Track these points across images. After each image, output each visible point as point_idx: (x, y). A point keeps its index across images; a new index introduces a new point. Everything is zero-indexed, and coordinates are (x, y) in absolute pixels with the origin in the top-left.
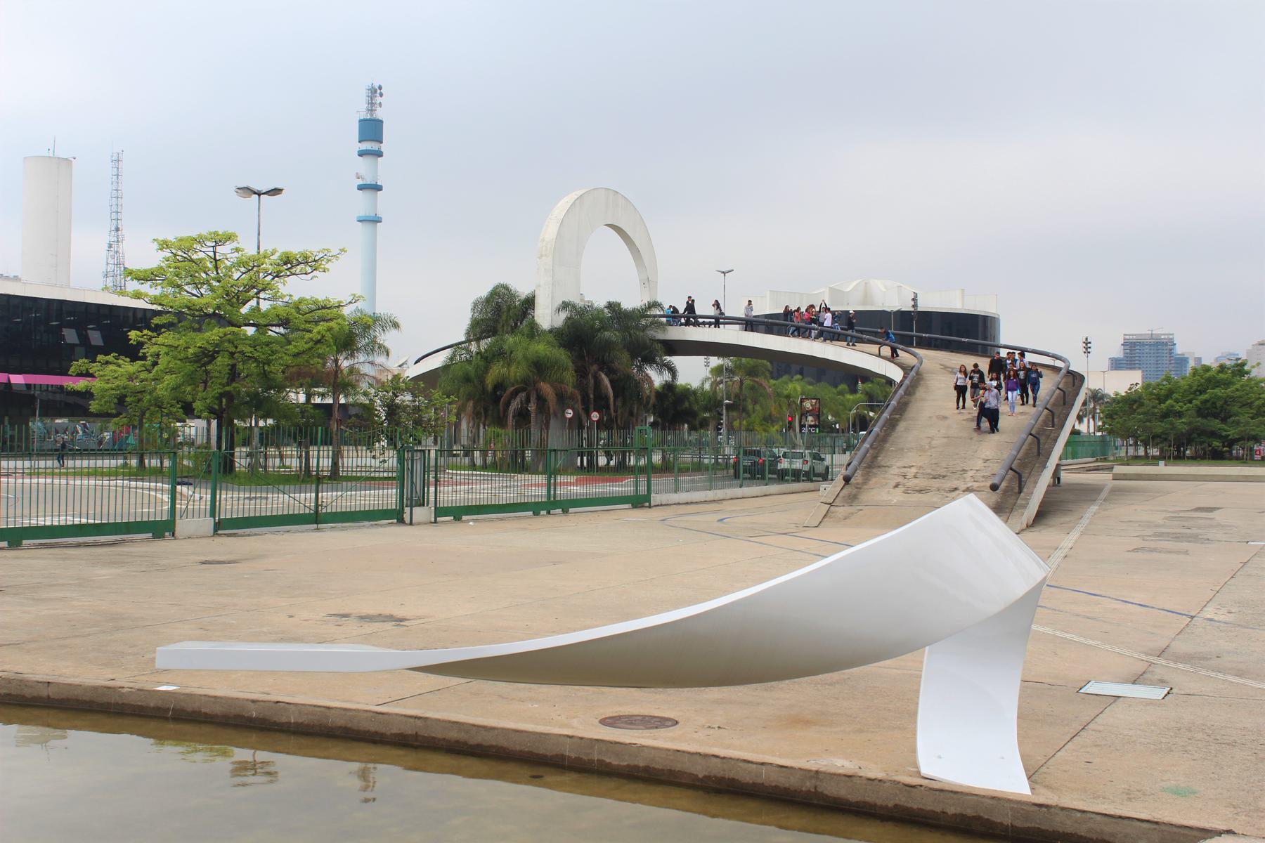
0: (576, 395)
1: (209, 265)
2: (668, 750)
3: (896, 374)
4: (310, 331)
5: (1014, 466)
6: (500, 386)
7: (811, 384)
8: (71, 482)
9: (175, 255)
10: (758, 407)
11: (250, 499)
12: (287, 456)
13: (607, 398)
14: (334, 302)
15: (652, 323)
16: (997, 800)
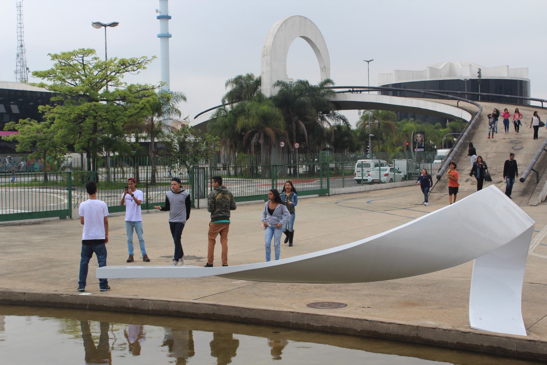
0: (286, 134)
1: (79, 67)
2: (342, 318)
3: (467, 117)
4: (138, 103)
5: (534, 168)
7: (419, 123)
8: (8, 190)
9: (61, 62)
10: (389, 138)
11: (108, 197)
12: (127, 173)
13: (303, 135)
14: (150, 86)
15: (328, 92)
16: (509, 339)
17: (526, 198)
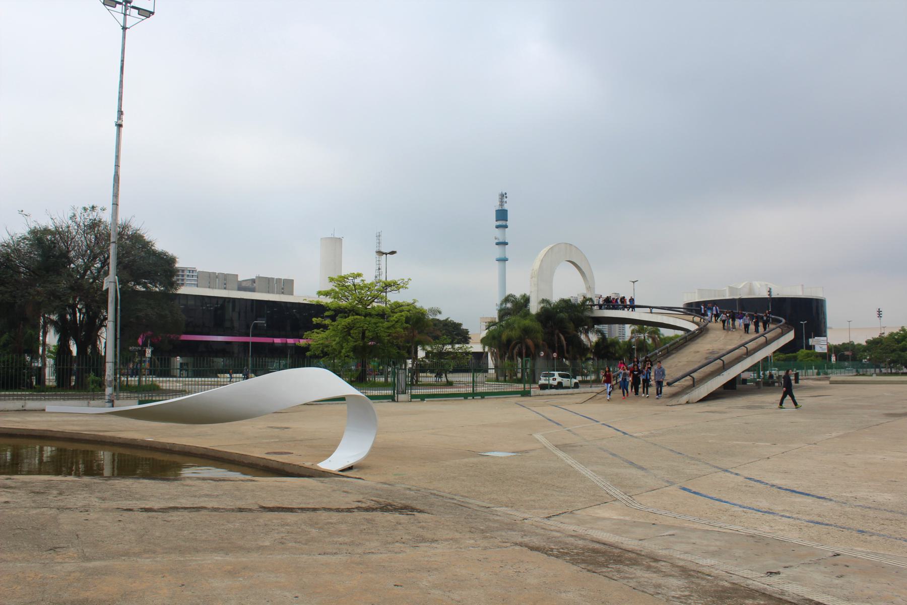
6: (509, 341)
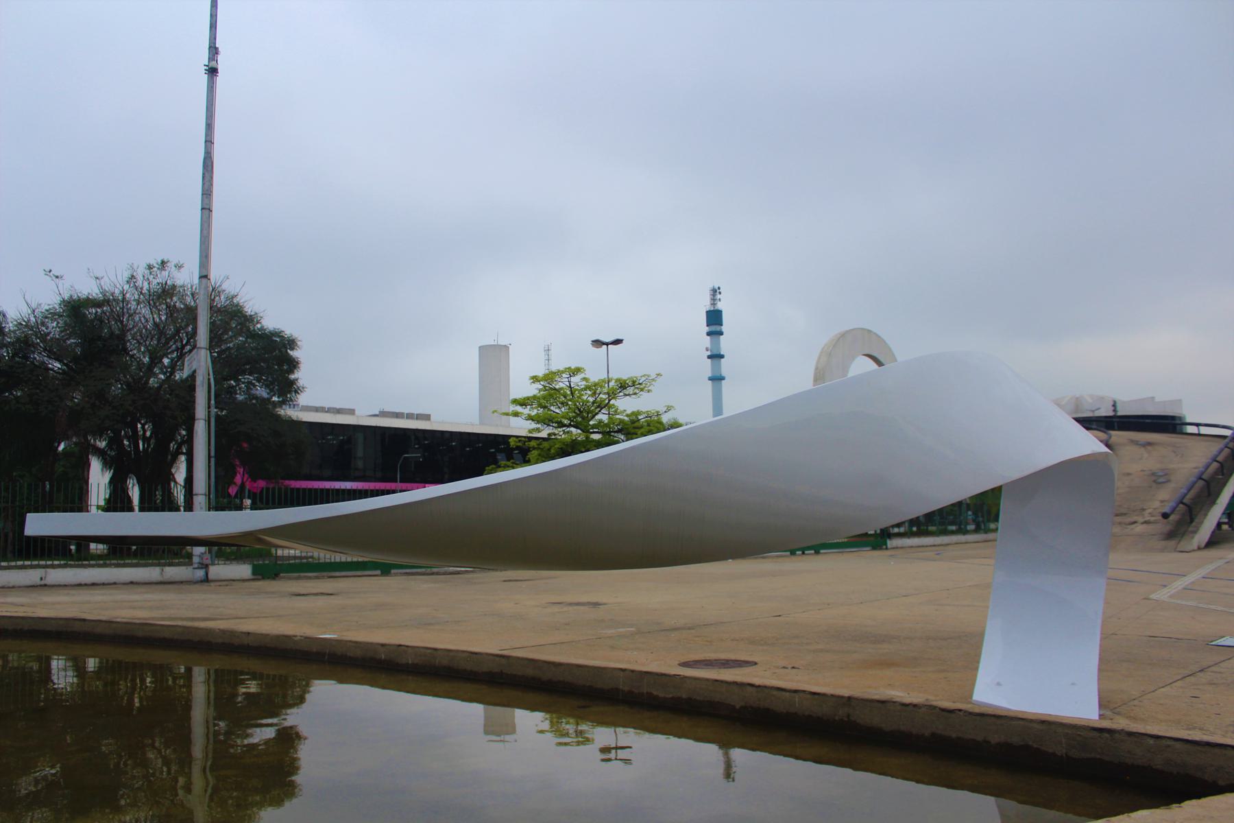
2: (707, 680)
16: (1048, 725)
17: (1172, 543)
